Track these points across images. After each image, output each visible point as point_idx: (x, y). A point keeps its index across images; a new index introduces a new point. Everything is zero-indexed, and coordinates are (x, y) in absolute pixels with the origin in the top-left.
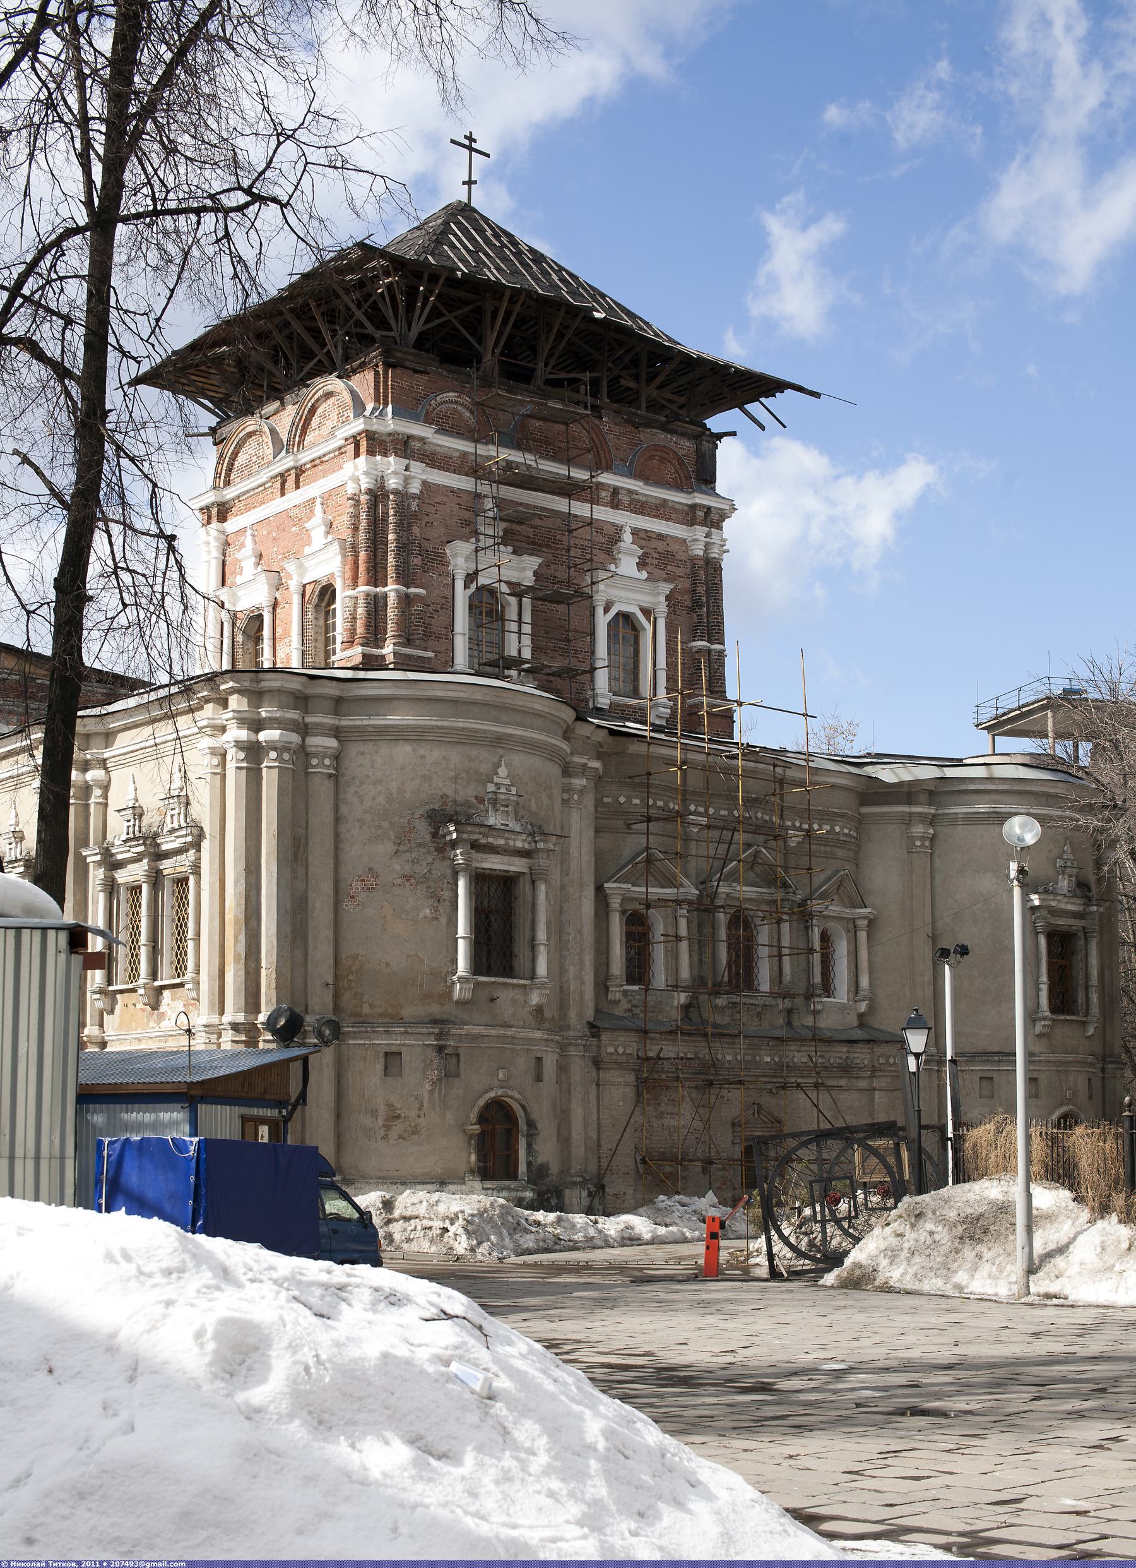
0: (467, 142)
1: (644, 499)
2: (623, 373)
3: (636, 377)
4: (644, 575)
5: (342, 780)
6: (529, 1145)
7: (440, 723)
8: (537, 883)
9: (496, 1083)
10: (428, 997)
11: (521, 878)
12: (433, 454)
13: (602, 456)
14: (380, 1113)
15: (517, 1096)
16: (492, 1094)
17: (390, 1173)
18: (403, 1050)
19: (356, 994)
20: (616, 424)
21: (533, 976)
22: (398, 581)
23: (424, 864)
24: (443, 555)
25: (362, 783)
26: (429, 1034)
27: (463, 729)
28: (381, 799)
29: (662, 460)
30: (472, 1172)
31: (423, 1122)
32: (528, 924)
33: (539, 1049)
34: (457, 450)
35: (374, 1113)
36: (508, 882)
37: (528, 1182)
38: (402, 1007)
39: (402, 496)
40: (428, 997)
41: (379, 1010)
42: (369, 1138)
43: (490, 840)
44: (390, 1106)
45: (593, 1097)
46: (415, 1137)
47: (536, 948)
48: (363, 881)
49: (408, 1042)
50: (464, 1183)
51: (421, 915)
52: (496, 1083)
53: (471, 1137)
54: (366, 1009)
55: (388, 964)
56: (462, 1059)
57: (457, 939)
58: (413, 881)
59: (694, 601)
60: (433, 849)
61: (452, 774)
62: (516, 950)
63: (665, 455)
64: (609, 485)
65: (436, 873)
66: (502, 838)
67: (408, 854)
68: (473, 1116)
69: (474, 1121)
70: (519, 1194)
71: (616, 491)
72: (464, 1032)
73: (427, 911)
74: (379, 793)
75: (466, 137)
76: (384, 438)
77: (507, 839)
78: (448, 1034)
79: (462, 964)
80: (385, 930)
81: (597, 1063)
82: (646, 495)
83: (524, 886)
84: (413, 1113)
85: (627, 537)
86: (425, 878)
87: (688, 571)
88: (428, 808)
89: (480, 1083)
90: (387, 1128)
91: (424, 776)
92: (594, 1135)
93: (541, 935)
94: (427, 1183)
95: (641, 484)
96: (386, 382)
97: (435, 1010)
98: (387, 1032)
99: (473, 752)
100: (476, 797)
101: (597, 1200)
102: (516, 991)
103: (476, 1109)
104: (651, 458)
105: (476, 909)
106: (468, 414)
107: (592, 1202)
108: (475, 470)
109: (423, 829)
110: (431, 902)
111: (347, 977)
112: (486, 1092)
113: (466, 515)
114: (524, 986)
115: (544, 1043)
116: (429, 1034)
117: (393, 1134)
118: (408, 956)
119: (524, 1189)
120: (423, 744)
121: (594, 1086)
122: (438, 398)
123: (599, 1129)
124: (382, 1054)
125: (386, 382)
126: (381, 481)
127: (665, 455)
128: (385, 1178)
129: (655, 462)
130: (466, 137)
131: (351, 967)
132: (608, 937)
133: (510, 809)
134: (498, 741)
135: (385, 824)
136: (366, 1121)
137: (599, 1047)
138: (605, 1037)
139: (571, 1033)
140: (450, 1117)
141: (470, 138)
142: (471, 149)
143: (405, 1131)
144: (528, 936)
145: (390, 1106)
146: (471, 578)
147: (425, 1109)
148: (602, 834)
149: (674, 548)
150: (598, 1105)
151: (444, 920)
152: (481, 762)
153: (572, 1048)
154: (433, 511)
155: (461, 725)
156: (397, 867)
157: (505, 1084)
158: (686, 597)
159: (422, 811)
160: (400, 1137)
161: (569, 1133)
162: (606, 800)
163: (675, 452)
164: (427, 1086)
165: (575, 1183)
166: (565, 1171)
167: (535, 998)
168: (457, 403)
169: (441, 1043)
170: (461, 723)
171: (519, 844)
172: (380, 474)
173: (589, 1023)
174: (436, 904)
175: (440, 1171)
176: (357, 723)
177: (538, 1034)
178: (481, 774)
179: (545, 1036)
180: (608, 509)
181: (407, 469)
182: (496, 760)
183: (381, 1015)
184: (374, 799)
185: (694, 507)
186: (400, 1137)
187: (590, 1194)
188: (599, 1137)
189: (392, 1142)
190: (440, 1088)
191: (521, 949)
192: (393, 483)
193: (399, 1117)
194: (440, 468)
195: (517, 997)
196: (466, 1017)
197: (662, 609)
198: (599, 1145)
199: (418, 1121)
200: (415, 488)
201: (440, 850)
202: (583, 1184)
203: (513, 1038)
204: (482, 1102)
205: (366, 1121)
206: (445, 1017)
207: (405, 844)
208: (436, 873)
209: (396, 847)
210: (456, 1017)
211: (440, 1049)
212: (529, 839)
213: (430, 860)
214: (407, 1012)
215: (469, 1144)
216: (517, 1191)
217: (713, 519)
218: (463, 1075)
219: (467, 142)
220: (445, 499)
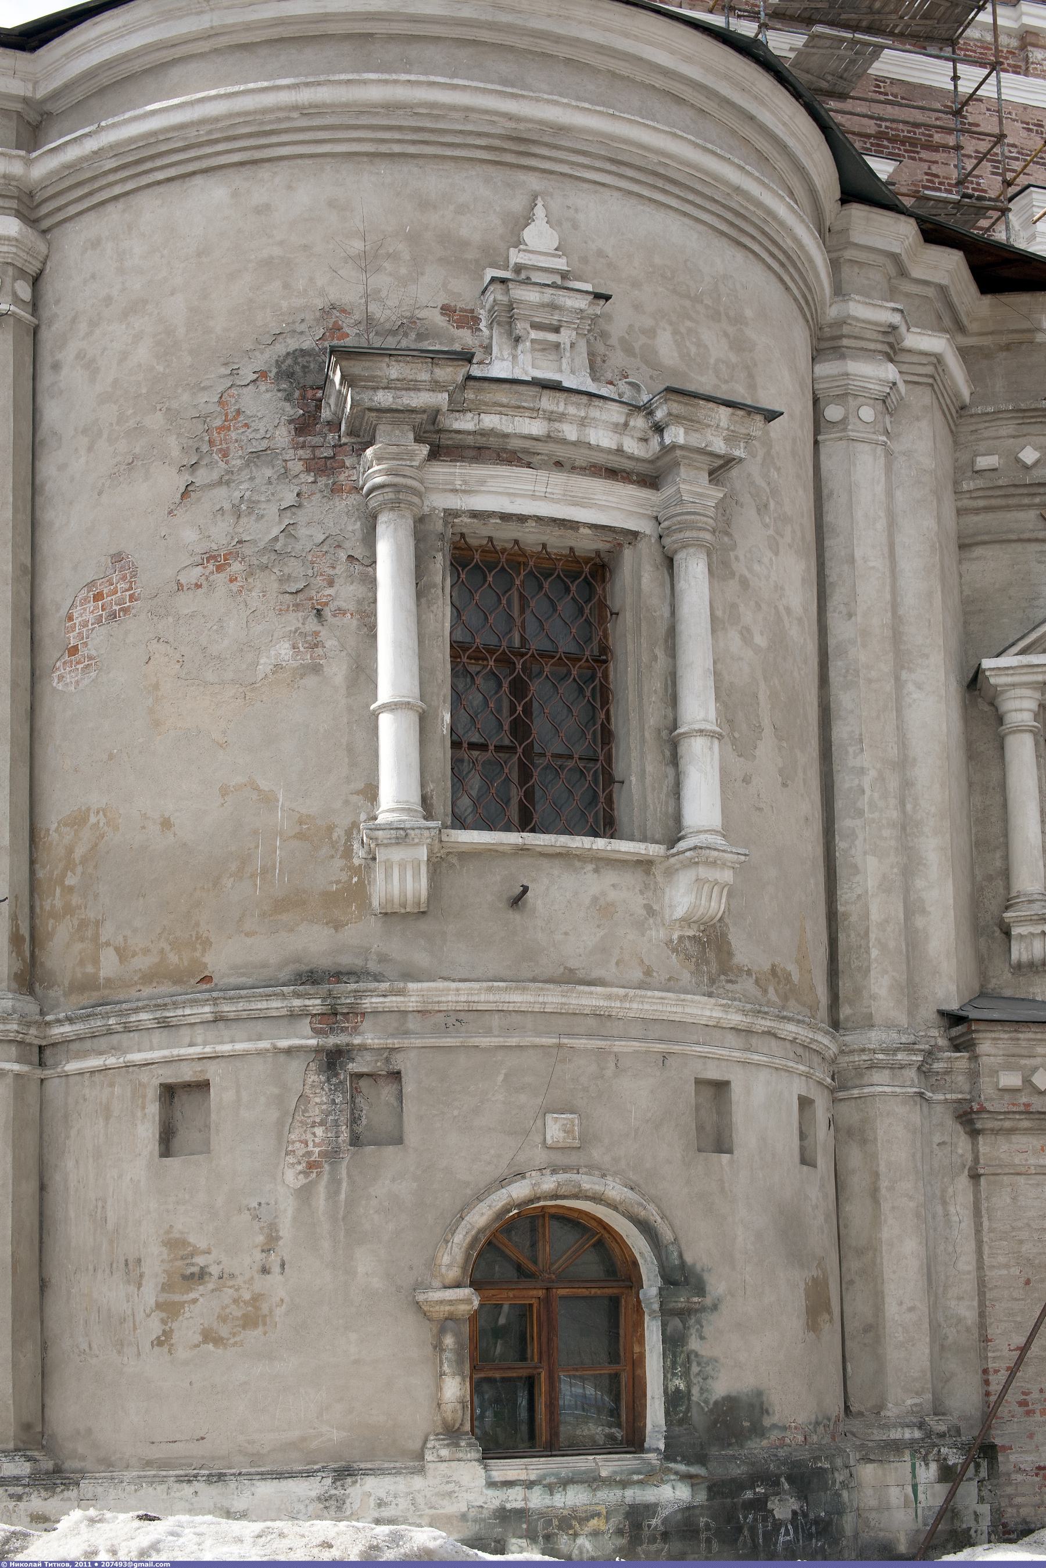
5: (45, 334)
6: (673, 1343)
7: (305, 96)
8: (678, 558)
9: (540, 1156)
10: (289, 905)
11: (627, 553)
14: (146, 1268)
15: (615, 1190)
16: (519, 1191)
17: (179, 1449)
18: (214, 1073)
19: (83, 924)
21: (674, 834)
23: (272, 510)
25: (93, 324)
26: (293, 1016)
27: (391, 107)
28: (142, 354)
30: (451, 1434)
31: (276, 1286)
32: (655, 684)
33: (719, 1059)
35: (132, 1269)
36: (583, 578)
37: (669, 1454)
38: (207, 944)
40: (289, 905)
41: (142, 963)
42: (120, 1345)
43: (490, 421)
44: (175, 1244)
45: (960, 1210)
46: (253, 1336)
47: (683, 749)
48: (98, 597)
49: (226, 1048)
50: (421, 1471)
51: (265, 664)
52: (540, 1156)
53: (445, 1323)
54: (109, 965)
55: (166, 824)
56: (409, 1087)
57: (375, 716)
58: (236, 567)
60: (297, 467)
61: (358, 245)
62: (619, 770)
65: (309, 534)
66: (535, 412)
67: (222, 492)
68: (452, 1258)
69: (453, 1273)
70: (632, 1495)
72: (411, 1003)
73: (284, 650)
74: (138, 338)
77: (551, 417)
78: (355, 1013)
79: (395, 789)
80: (157, 724)
81: (968, 1118)
83: (636, 577)
84: (247, 1261)
86: (277, 552)
88: (280, 349)
89: (477, 1155)
90: (170, 1310)
91: (268, 263)
92: (967, 1311)
93: (698, 707)
94: (292, 1475)
97: (314, 942)
98: (164, 1024)
99: (432, 182)
100: (446, 310)
101: (969, 1491)
102: (610, 877)
103: (461, 1239)
105: (459, 651)
107: (951, 1495)
109: (267, 413)
110: (294, 620)
111: (61, 880)
112: (502, 1182)
114: (645, 864)
115: (731, 1038)
116: (293, 1016)
117: (187, 1329)
118: (224, 791)
119: (651, 1477)
120: (264, 173)
121: (963, 1181)
123: (981, 1294)
124: (152, 1093)
128: (165, 1464)
131: (70, 851)
132: (1005, 805)
133: (565, 337)
134: (517, 149)
135: (156, 421)
136: (112, 1293)
137: (974, 1075)
138: (991, 1046)
139: (875, 1038)
140: (367, 1265)
143: (223, 1319)
144: (654, 716)
145: (175, 1244)
147: (284, 1249)
148: (978, 551)
150: (978, 1231)
151: (337, 671)
152: (462, 209)
153: (877, 1077)
155: (375, 94)
156: (190, 535)
157: (573, 1159)
159: (264, 359)
160: (209, 1336)
161: (878, 1308)
162: (984, 462)
164: (290, 1175)
165: (896, 1447)
166: (852, 1410)
167: (684, 898)
169: (332, 1041)
170: (374, 90)
171: (602, 438)
173: (942, 1013)
174: (312, 625)
175: (336, 1435)
176: (72, 154)
177: (703, 1009)
178: (465, 244)
179: (735, 1019)
182: (517, 204)
183: (149, 977)
184: (124, 356)
186: (209, 1336)
187: (947, 1474)
188: (982, 1315)
189: (182, 1354)
190: (335, 1182)
191: (637, 763)
193: (202, 1275)
195: (613, 895)
196: (421, 958)
198: (985, 1339)
199: (261, 1284)
201: (324, 466)
202: (923, 1448)
203: (602, 1017)
204: (481, 1216)
205: (112, 1293)
206: (346, 961)
207: (211, 465)
208: (309, 534)
209: (187, 478)
210: (383, 959)
211: (333, 1060)
212: (639, 422)
213: (290, 499)
214: (224, 957)
215: (438, 1347)
216: (624, 1484)
218: (412, 1137)
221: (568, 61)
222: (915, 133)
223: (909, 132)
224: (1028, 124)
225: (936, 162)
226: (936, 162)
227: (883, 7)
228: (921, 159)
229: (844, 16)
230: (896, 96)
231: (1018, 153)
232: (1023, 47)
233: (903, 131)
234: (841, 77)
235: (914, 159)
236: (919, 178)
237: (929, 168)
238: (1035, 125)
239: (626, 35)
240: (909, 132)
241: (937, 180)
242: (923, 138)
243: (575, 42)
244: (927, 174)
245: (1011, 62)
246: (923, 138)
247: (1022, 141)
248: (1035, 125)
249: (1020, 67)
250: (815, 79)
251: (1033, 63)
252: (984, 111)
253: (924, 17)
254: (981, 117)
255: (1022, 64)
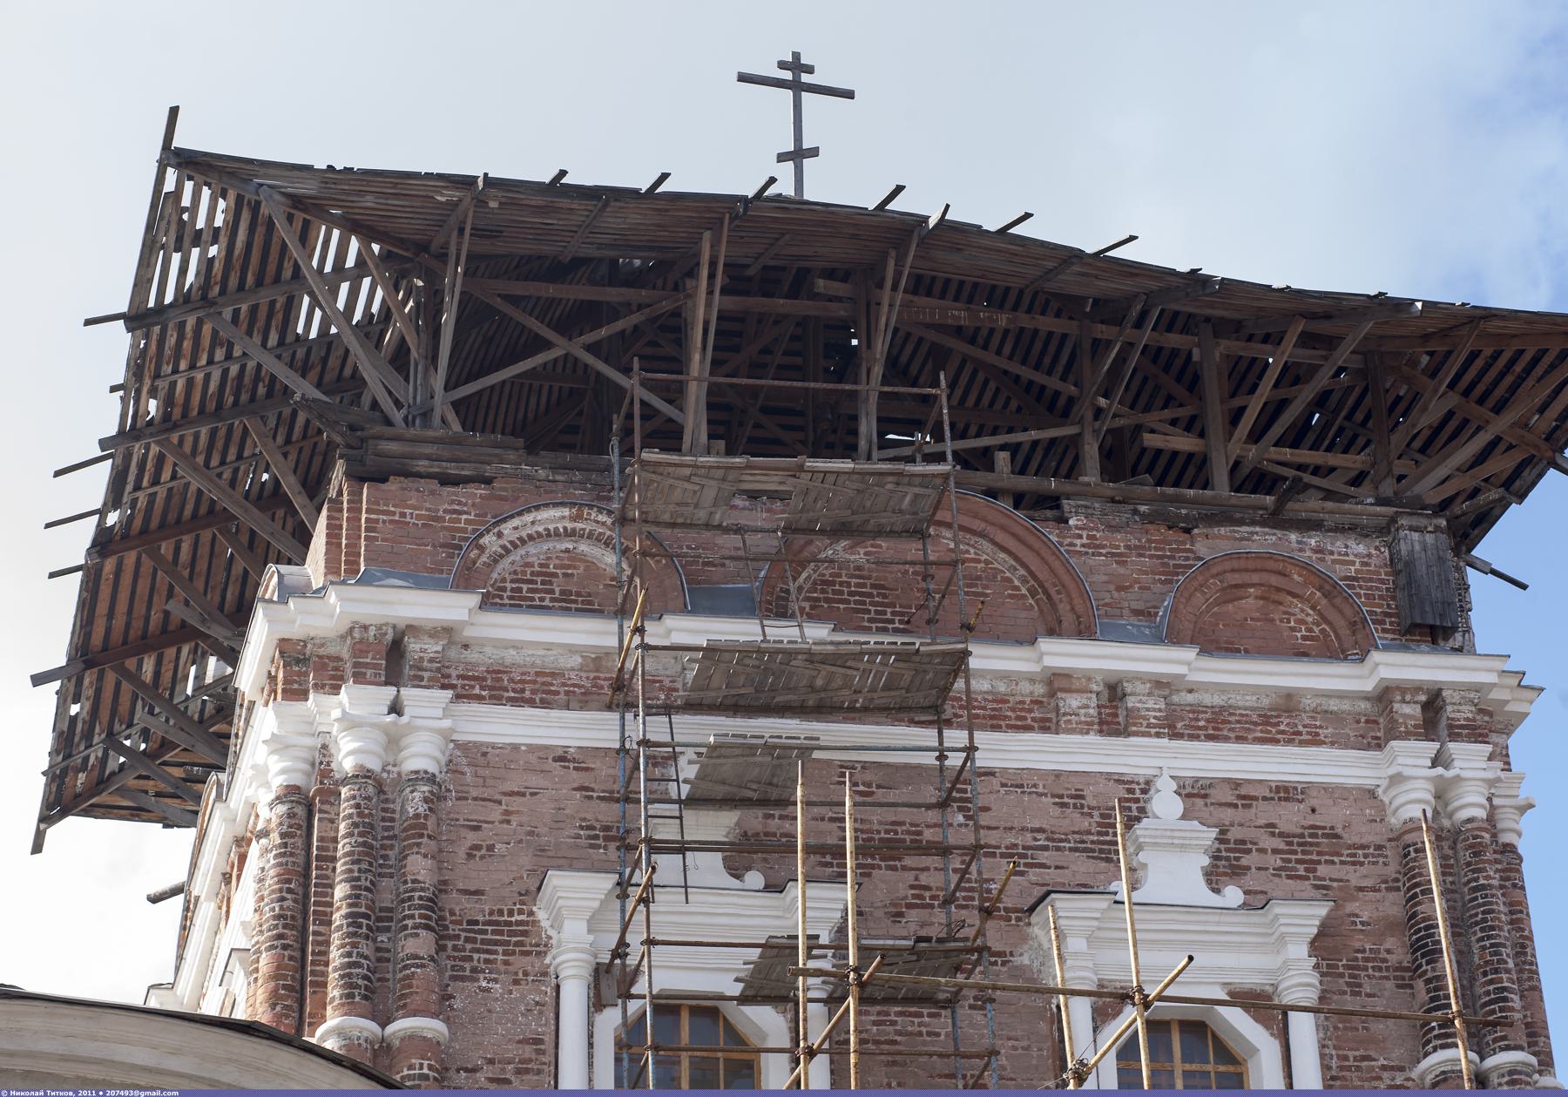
0: (787, 75)
1: (1218, 700)
2: (1152, 419)
3: (1191, 425)
4: (1233, 895)
12: (497, 672)
13: (1063, 608)
20: (1112, 528)
22: (350, 1004)
24: (529, 927)
29: (1271, 596)
34: (572, 649)
39: (377, 787)
59: (1415, 947)
63: (1274, 580)
64: (1088, 676)
71: (1115, 691)
75: (782, 65)
76: (332, 650)
82: (1222, 688)
85: (1166, 804)
87: (1392, 870)
95: (1189, 653)
96: (354, 520)
104: (1233, 593)
106: (610, 558)
108: (616, 691)
113: (609, 813)
122: (507, 528)
125: (354, 520)
126: (321, 764)
127: (1274, 580)
129: (1250, 603)
130: (782, 65)
141: (796, 65)
142: (797, 87)
146: (611, 979)
149: (1331, 816)
154: (495, 814)
158: (1390, 943)
163: (1305, 567)
168: (571, 534)
172: (318, 742)
180: (1093, 738)
181: (396, 708)
185: (1385, 695)
192: (346, 760)
194: (519, 701)
197: (1299, 980)
200: (421, 755)
217: (1488, 724)
219: (787, 75)
220: (534, 781)
221: (27, 1074)
222: (896, 833)
223: (887, 832)
224: (1061, 797)
225: (927, 869)
226: (927, 869)
227: (829, 682)
228: (904, 868)
229: (778, 699)
230: (869, 785)
231: (1047, 839)
232: (1052, 694)
233: (879, 832)
234: (770, 784)
235: (894, 868)
236: (902, 893)
237: (916, 879)
238: (1072, 797)
239: (94, 1038)
240: (887, 832)
241: (927, 894)
242: (908, 838)
243: (30, 1055)
244: (912, 887)
245: (1037, 715)
246: (908, 838)
247: (1053, 821)
248: (1072, 797)
249: (1049, 720)
250: (734, 790)
251: (1065, 714)
252: (997, 787)
253: (887, 688)
254: (993, 797)
255: (1052, 715)
